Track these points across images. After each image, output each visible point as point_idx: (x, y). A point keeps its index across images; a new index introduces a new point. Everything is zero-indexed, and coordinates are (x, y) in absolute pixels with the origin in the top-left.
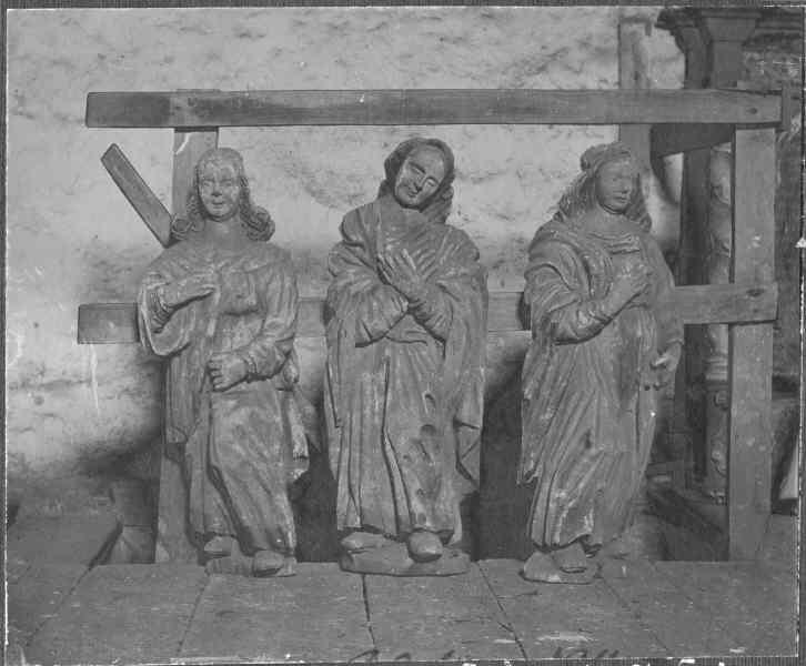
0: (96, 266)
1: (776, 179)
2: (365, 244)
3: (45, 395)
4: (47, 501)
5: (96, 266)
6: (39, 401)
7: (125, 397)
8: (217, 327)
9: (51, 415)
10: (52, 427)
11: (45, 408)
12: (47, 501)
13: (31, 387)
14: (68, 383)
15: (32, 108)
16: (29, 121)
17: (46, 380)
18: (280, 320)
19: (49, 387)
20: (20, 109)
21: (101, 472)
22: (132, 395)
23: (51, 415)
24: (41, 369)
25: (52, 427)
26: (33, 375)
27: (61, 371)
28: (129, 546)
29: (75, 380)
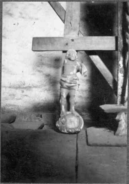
0: (39, 56)
1: (61, 101)
2: (41, 130)
3: (25, 91)
4: (23, 117)
5: (39, 56)
6: (23, 92)
7: (46, 91)
8: (69, 114)
9: (26, 95)
10: (26, 98)
11: (24, 94)
12: (23, 117)
13: (21, 88)
14: (30, 87)
15: (24, 15)
16: (23, 19)
17: (25, 86)
18: (85, 71)
19: (26, 88)
20: (21, 16)
21: (83, 91)
22: (48, 91)
23: (26, 95)
24: (23, 83)
25: (26, 98)
26: (21, 85)
27: (29, 84)
28: (45, 129)
29: (32, 86)
